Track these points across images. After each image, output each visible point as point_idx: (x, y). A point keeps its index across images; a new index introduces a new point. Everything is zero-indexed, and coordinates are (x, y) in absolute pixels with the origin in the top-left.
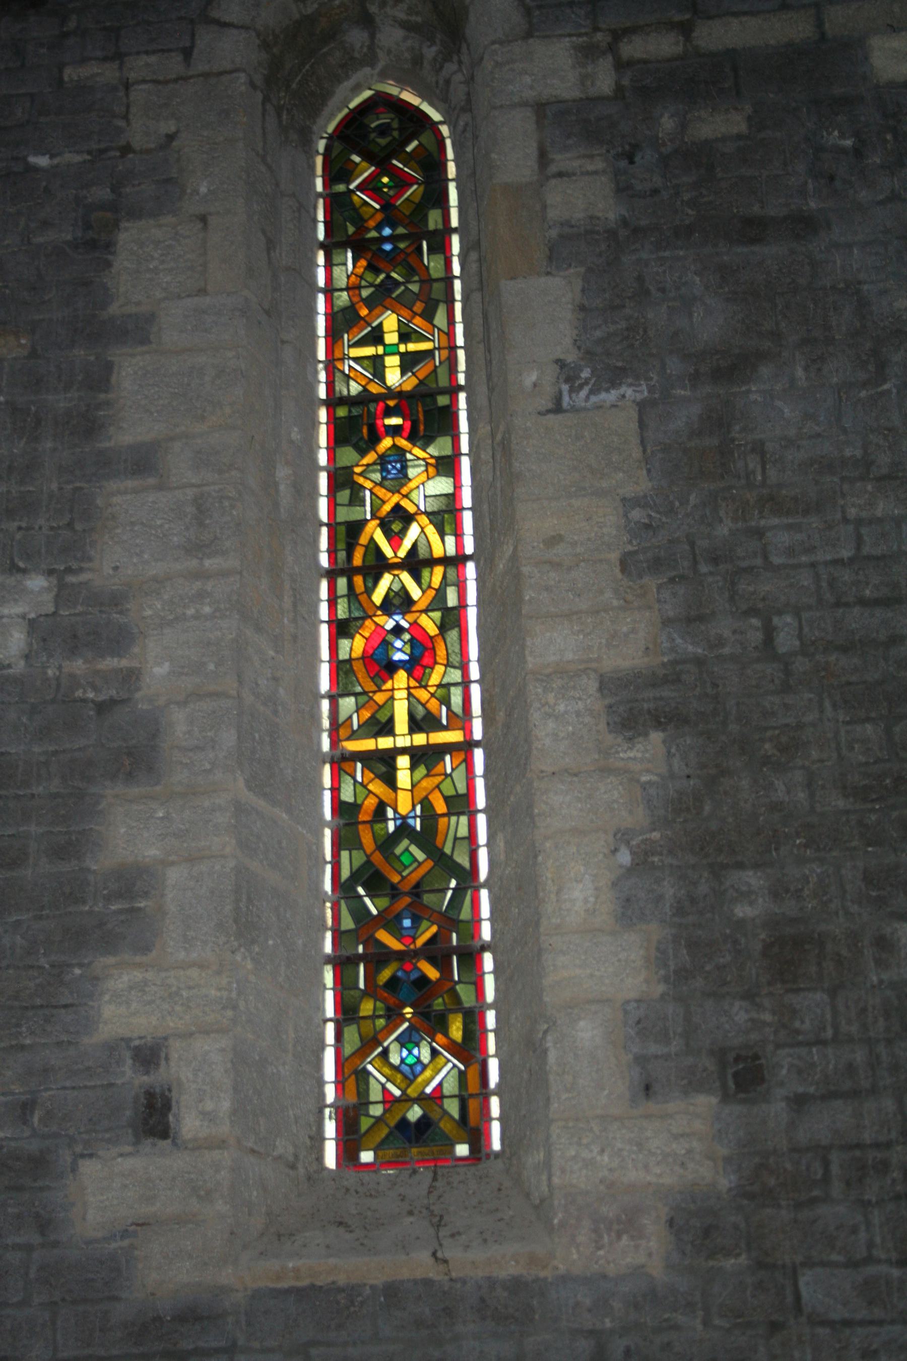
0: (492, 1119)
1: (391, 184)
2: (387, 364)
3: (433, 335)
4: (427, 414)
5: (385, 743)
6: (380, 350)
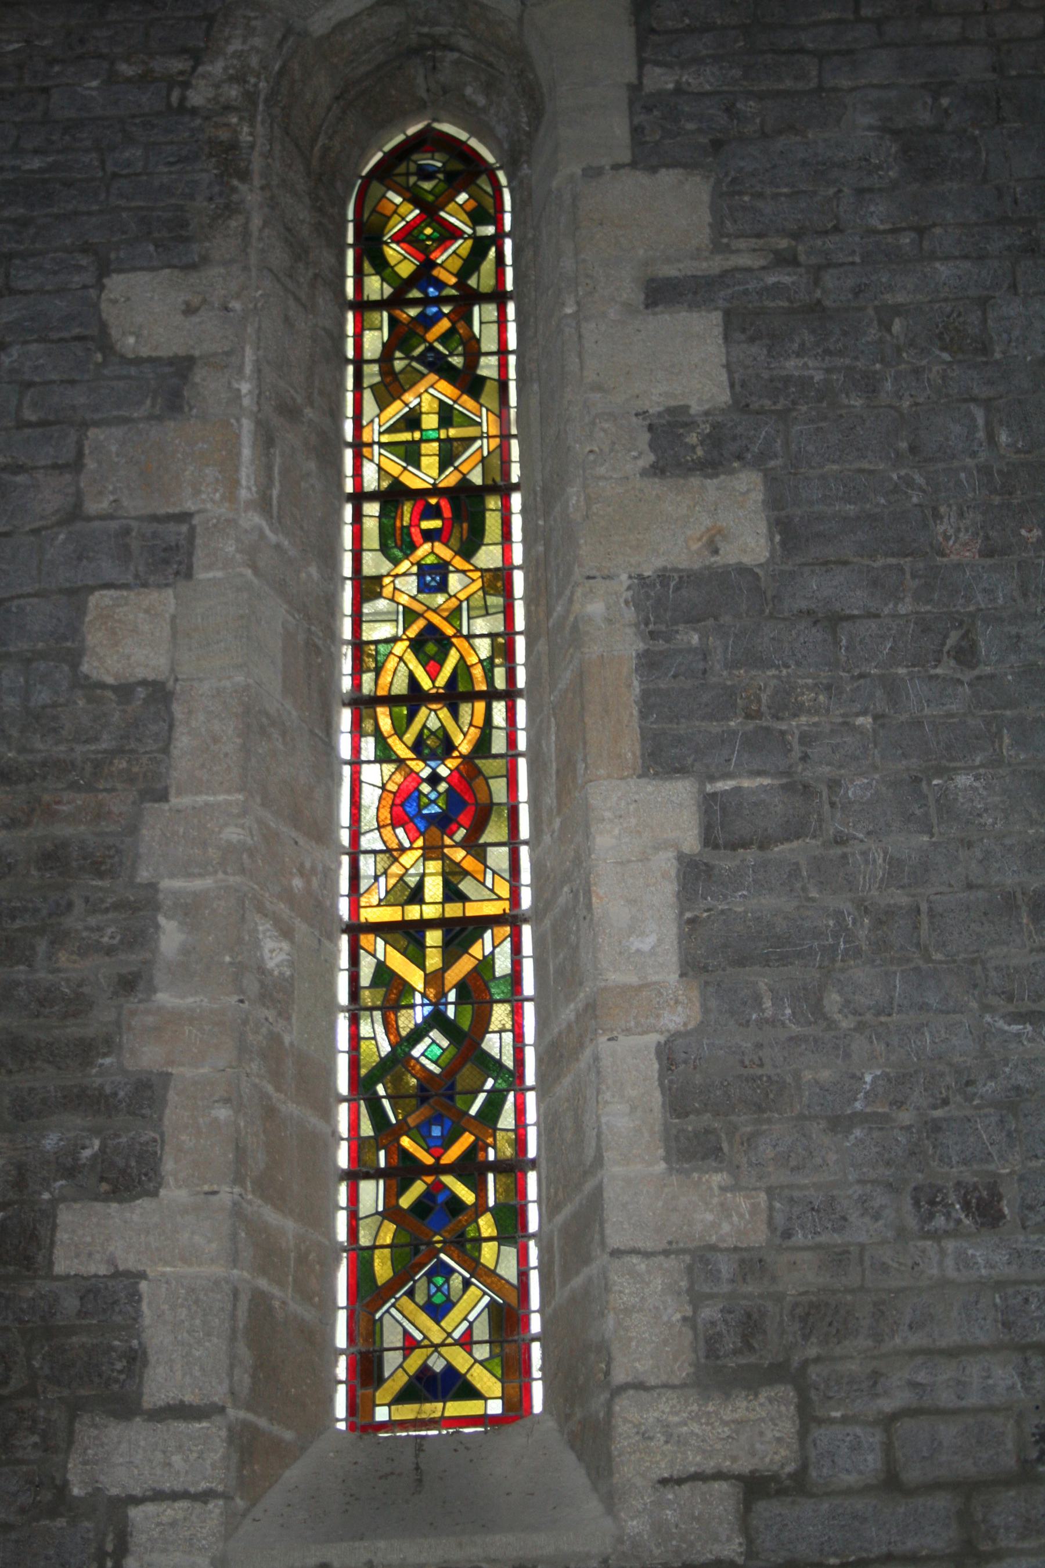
0: (533, 1045)
1: (436, 235)
2: (423, 452)
3: (480, 417)
4: (464, 511)
5: (413, 912)
6: (417, 435)
